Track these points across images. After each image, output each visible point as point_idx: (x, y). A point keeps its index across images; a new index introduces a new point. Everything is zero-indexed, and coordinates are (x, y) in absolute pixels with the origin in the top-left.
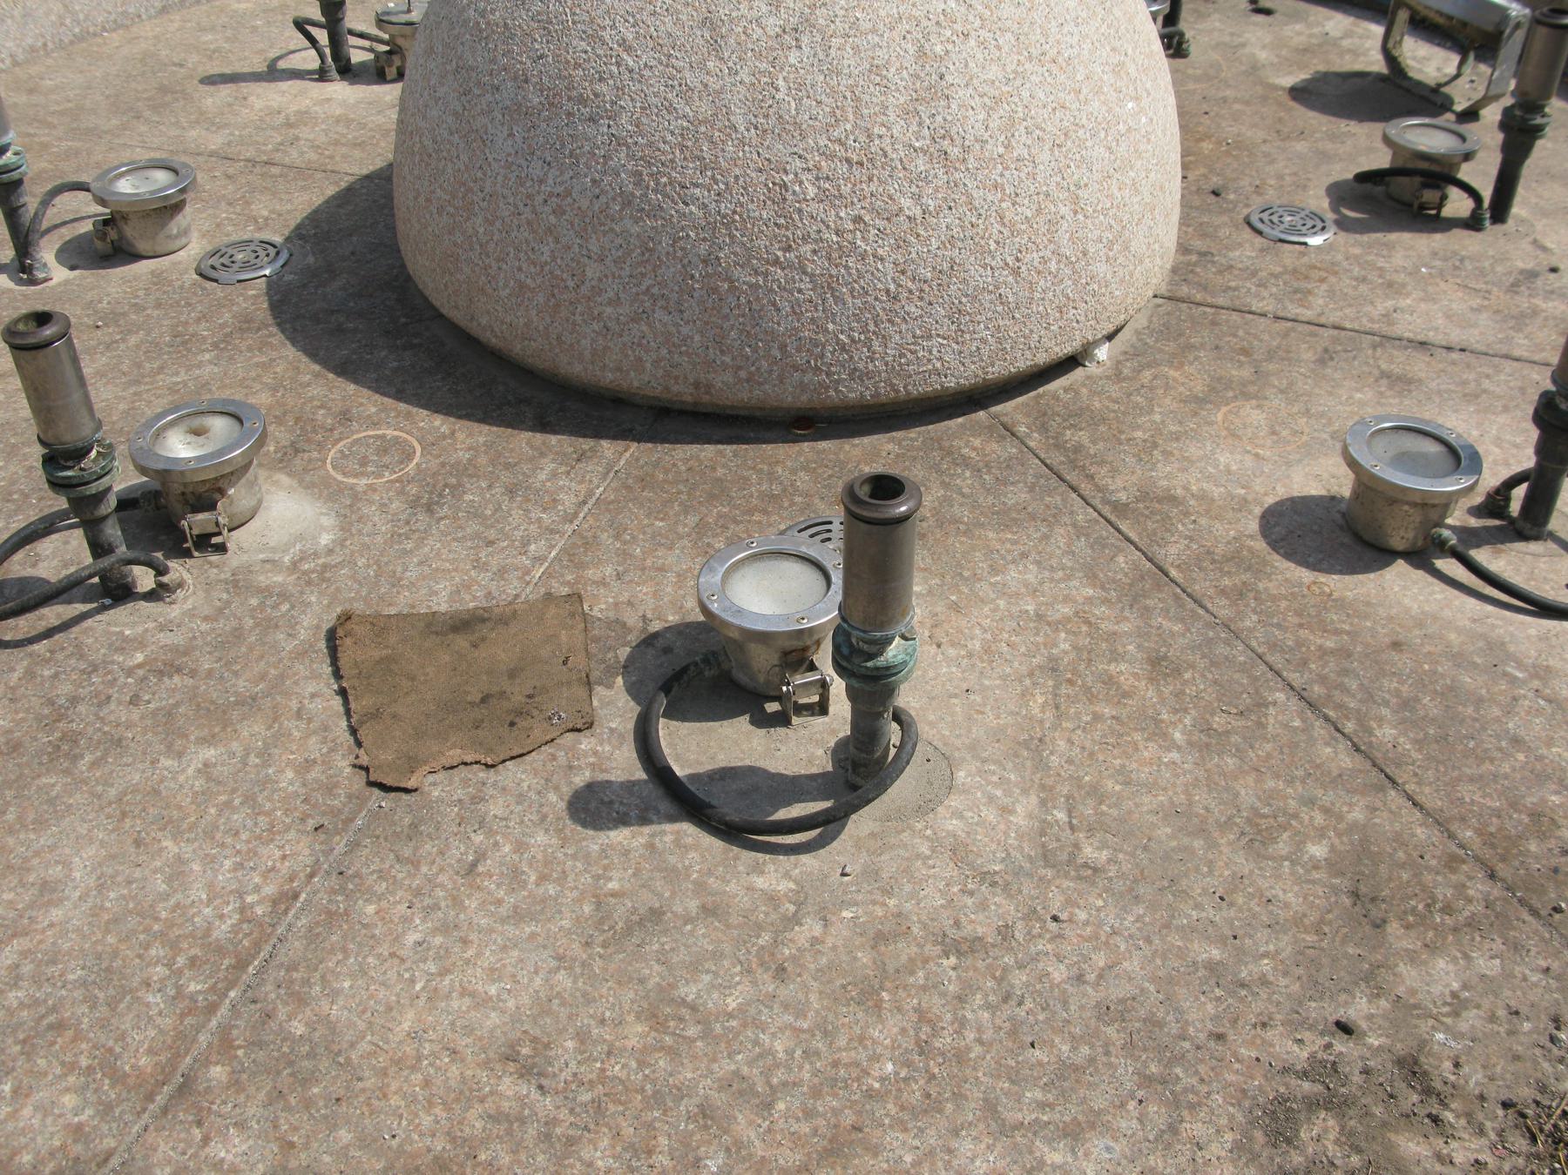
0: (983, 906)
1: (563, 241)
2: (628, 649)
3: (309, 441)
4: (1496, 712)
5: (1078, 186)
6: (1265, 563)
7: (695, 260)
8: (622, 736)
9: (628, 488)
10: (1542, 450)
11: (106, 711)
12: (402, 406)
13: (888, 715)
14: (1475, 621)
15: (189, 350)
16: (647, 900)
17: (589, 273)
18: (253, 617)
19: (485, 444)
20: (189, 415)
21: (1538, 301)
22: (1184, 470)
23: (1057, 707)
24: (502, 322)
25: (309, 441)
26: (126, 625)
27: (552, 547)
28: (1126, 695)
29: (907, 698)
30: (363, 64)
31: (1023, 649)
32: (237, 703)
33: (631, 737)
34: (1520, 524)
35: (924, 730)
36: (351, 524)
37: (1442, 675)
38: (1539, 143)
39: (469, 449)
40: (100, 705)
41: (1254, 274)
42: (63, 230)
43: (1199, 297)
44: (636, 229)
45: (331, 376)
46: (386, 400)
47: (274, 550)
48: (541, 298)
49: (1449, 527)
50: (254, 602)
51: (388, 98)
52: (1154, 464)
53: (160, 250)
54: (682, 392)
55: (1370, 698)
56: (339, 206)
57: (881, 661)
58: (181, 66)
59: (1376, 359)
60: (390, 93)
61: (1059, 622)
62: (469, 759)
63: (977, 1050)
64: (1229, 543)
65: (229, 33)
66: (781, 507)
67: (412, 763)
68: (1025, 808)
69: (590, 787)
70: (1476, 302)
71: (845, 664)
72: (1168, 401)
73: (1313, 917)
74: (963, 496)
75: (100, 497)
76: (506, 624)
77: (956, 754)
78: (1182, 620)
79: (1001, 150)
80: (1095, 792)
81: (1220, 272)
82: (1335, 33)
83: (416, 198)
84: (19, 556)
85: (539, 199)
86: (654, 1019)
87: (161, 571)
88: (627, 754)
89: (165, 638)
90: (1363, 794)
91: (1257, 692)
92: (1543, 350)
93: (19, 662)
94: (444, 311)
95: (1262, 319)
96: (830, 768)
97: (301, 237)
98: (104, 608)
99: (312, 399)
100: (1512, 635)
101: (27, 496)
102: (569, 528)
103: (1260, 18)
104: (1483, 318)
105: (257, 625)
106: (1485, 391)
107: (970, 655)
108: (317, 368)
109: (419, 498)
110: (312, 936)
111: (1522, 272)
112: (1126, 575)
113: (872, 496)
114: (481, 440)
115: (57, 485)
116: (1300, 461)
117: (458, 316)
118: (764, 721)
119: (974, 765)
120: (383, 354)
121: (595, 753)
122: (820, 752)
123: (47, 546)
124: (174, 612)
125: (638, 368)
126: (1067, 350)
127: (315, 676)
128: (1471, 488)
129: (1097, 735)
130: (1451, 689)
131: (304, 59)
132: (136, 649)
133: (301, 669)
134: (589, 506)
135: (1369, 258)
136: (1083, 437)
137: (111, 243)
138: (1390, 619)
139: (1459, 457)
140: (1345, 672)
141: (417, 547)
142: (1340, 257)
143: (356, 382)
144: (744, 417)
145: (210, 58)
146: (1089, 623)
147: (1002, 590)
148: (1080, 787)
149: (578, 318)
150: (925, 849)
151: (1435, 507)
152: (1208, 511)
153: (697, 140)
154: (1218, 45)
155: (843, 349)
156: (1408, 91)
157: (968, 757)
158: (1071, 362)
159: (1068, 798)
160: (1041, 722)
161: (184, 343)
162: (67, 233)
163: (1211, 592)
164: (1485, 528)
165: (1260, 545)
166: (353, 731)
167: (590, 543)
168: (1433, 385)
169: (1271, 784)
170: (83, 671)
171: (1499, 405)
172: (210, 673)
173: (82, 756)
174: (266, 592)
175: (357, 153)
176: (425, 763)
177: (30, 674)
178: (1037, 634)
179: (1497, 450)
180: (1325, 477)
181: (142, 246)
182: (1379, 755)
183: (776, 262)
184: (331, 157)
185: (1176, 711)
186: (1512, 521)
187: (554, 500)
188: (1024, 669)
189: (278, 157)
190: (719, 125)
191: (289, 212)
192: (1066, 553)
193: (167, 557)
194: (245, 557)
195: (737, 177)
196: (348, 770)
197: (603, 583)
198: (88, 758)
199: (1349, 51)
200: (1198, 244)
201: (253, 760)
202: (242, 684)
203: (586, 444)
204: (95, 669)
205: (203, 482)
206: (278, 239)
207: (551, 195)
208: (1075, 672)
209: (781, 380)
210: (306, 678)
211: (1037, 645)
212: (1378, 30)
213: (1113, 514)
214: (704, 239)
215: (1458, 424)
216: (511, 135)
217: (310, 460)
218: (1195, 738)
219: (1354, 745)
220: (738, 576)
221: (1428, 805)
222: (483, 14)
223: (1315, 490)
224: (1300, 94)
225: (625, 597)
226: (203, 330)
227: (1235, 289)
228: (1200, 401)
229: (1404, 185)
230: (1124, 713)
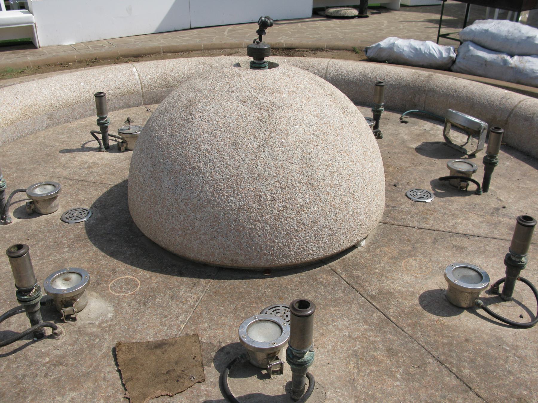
1: (188, 214)
2: (215, 353)
3: (102, 280)
4: (502, 362)
5: (354, 192)
6: (422, 314)
7: (232, 220)
8: (215, 384)
9: (211, 296)
10: (507, 273)
11: (36, 380)
12: (133, 268)
13: (305, 376)
14: (491, 330)
15: (60, 248)
17: (196, 224)
18: (86, 344)
19: (162, 281)
20: (63, 274)
21: (500, 218)
22: (392, 283)
23: (358, 368)
24: (167, 240)
25: (102, 280)
26: (42, 347)
27: (187, 317)
28: (380, 363)
29: (311, 370)
30: (113, 146)
31: (345, 348)
32: (82, 375)
33: (218, 384)
34: (503, 296)
35: (316, 379)
36: (118, 310)
37: (483, 350)
38: (496, 168)
39: (157, 283)
40: (34, 378)
42: (15, 205)
43: (393, 222)
44: (212, 211)
45: (108, 257)
46: (127, 265)
47: (92, 319)
48: (180, 232)
49: (481, 299)
51: (122, 158)
52: (383, 281)
53: (48, 212)
54: (228, 263)
55: (460, 359)
56: (107, 196)
57: (303, 360)
58: (53, 146)
59: (451, 241)
60: (121, 156)
61: (356, 338)
62: (164, 394)
64: (409, 307)
65: (69, 135)
66: (262, 301)
71: (291, 361)
72: (386, 259)
74: (322, 295)
75: (35, 305)
76: (173, 345)
77: (326, 386)
78: (396, 336)
79: (330, 182)
81: (399, 213)
82: (428, 129)
83: (137, 198)
84: (3, 323)
85: (180, 200)
87: (54, 328)
88: (217, 390)
89: (56, 352)
90: (461, 394)
91: (423, 359)
92: (504, 235)
93: (4, 362)
94: (146, 235)
95: (414, 229)
96: (285, 393)
97: (95, 207)
98: (34, 342)
99: (102, 265)
100: (504, 335)
101: (5, 301)
102: (192, 310)
103: (404, 124)
104: (484, 225)
105: (88, 347)
106: (487, 250)
107: (328, 351)
108: (103, 254)
109: (141, 300)
111: (494, 208)
112: (377, 320)
113: (299, 307)
114: (161, 279)
115: (20, 301)
116: (430, 278)
117: (151, 237)
118: (262, 377)
119: (332, 390)
120: (125, 249)
121: (206, 390)
122: (281, 387)
123: (13, 319)
125: (213, 255)
126: (353, 244)
127: (109, 365)
128: (487, 286)
129: (372, 377)
130: (486, 355)
131: (94, 144)
132: (46, 357)
133: (104, 363)
134: (198, 302)
135: (446, 206)
136: (359, 273)
137: (32, 210)
138: (464, 331)
139: (481, 276)
140: (451, 351)
141: (141, 318)
142: (436, 206)
143: (117, 259)
144: (248, 270)
145: (63, 144)
146: (366, 338)
147: (337, 328)
148: (368, 396)
149: (193, 239)
151: (475, 294)
152: (402, 297)
153: (232, 182)
154: (391, 134)
155: (280, 248)
156: (452, 148)
157: (330, 387)
159: (364, 400)
160: (353, 373)
161: (58, 245)
162: (17, 206)
163: (405, 325)
164: (492, 298)
165: (420, 308)
166: (124, 385)
167: (199, 316)
168: (470, 249)
169: (430, 391)
170: (27, 365)
171: (492, 254)
172: (72, 364)
173: (28, 397)
174: (90, 335)
175: (113, 177)
176: (149, 396)
177: (8, 367)
178: (349, 343)
179: (493, 270)
180: (437, 283)
181: (43, 211)
182: (465, 379)
183: (258, 221)
184: (104, 179)
185: (397, 367)
186: (500, 295)
187: (187, 301)
188: (346, 355)
190: (239, 177)
191: (91, 198)
192: (356, 314)
193: (56, 322)
194: (83, 322)
195: (245, 194)
196: (122, 399)
197: (204, 330)
198: (30, 398)
199: (433, 135)
200: (391, 204)
201: (89, 396)
202: (84, 368)
203: (196, 280)
204: (32, 364)
205: (69, 297)
206: (88, 208)
207: (184, 199)
208: (363, 355)
209: (260, 258)
210: (106, 366)
211: (350, 346)
214: (235, 214)
215: (479, 262)
217: (103, 287)
218: (404, 377)
219: (457, 376)
220: (251, 329)
221: (483, 396)
222: (160, 139)
223: (436, 288)
224: (419, 150)
226: (64, 240)
227: (404, 219)
229: (455, 182)
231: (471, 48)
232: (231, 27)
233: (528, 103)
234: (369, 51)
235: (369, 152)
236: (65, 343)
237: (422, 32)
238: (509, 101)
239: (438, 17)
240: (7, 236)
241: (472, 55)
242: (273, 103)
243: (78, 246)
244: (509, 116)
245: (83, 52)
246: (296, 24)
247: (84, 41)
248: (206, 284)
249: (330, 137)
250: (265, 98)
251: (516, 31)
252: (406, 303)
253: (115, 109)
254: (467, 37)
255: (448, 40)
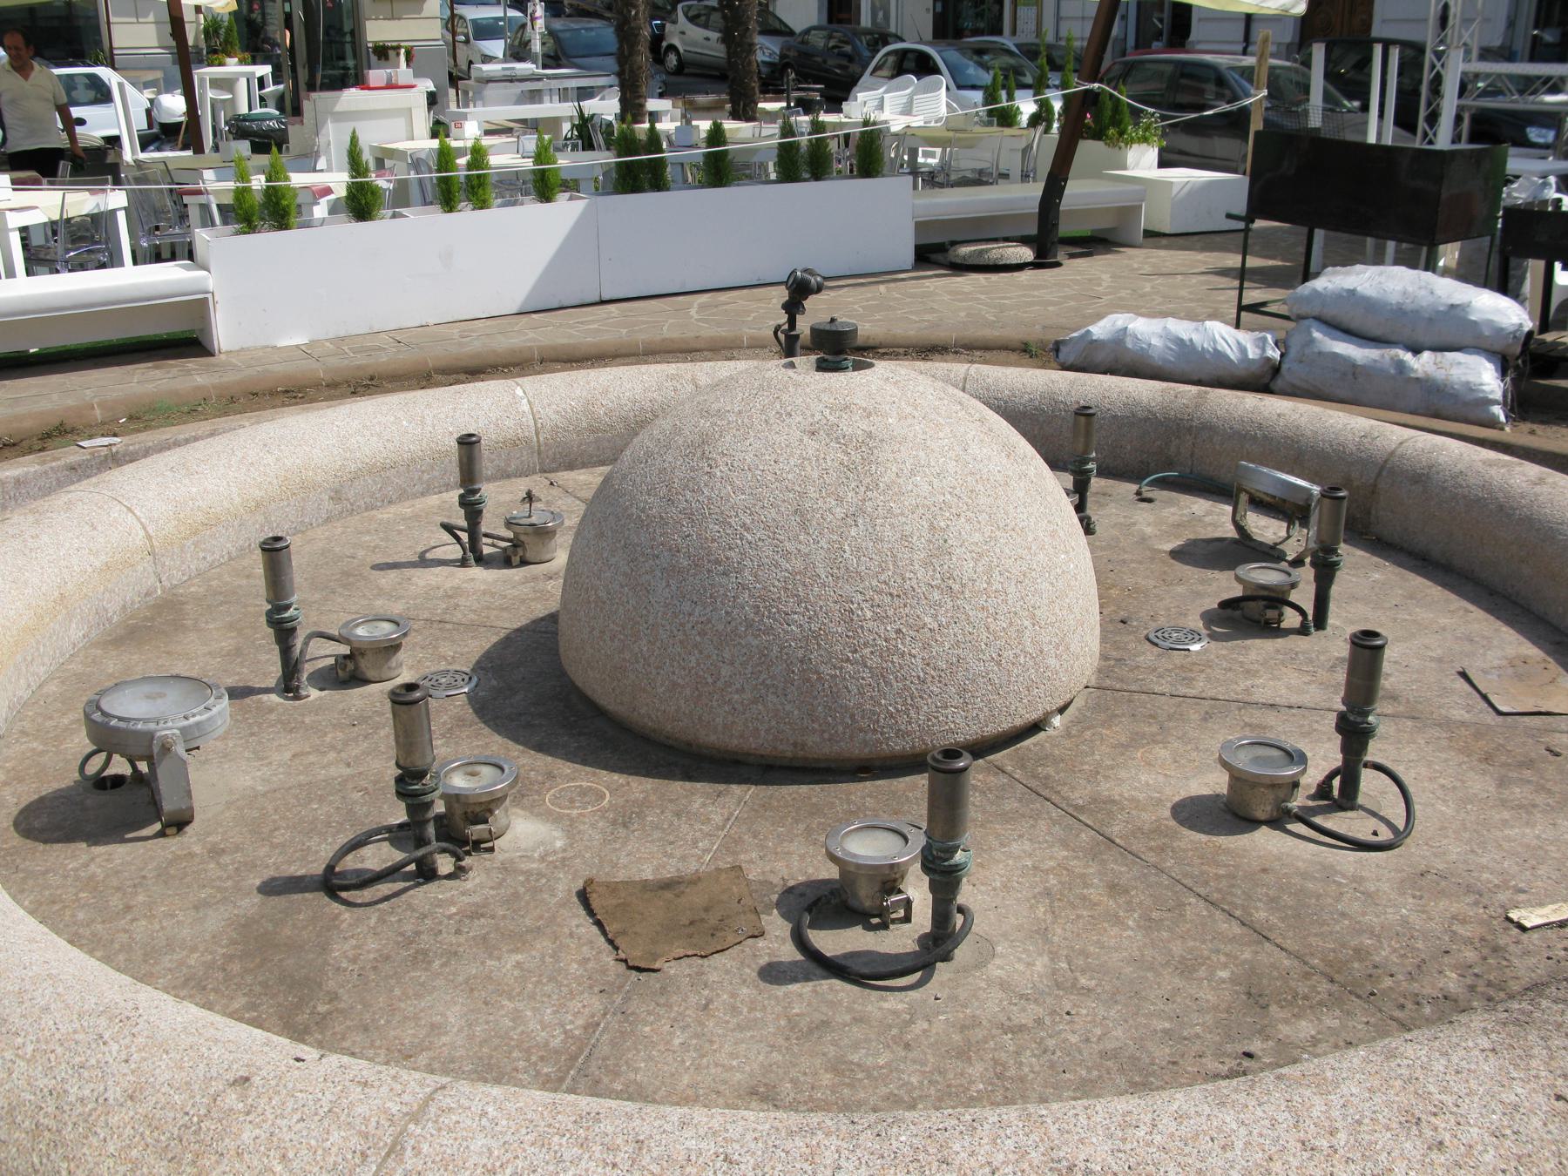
0: (1024, 1010)
4: (1330, 900)
8: (784, 940)
12: (588, 769)
16: (818, 1017)
17: (723, 672)
41: (1154, 670)
43: (1118, 686)
50: (521, 878)
54: (786, 750)
57: (952, 862)
63: (1031, 1076)
67: (655, 957)
68: (1041, 964)
69: (770, 965)
70: (1307, 678)
73: (1223, 1006)
80: (1084, 953)
82: (1199, 513)
84: (350, 857)
86: (835, 1070)
89: (466, 899)
98: (418, 885)
103: (1145, 505)
107: (995, 889)
110: (613, 1044)
119: (1006, 944)
123: (367, 851)
124: (469, 885)
126: (1033, 716)
136: (1050, 770)
139: (1295, 757)
140: (1233, 886)
147: (1010, 855)
150: (983, 985)
158: (1035, 727)
165: (1173, 823)
169: (1191, 944)
172: (504, 917)
174: (528, 873)
175: (505, 615)
177: (382, 921)
180: (1215, 783)
181: (370, 674)
183: (848, 660)
186: (1335, 801)
188: (1030, 895)
189: (447, 617)
197: (751, 861)
201: (548, 959)
202: (528, 922)
203: (722, 787)
206: (467, 670)
212: (1229, 509)
213: (1074, 813)
216: (668, 585)
223: (1206, 791)
224: (1176, 554)
225: (768, 868)
228: (1126, 747)
230: (1096, 914)
231: (1317, 335)
232: (705, 298)
233: (1420, 445)
234: (1064, 350)
235: (1061, 533)
236: (481, 885)
237: (1198, 300)
238: (1377, 442)
239: (1234, 261)
240: (307, 720)
241: (1320, 353)
242: (870, 435)
243: (464, 735)
244: (1379, 474)
245: (334, 362)
246: (873, 288)
247: (331, 336)
248: (740, 796)
249: (982, 500)
250: (854, 425)
251: (1423, 292)
252: (1144, 816)
253: (504, 475)
254: (1304, 310)
255: (1267, 318)
